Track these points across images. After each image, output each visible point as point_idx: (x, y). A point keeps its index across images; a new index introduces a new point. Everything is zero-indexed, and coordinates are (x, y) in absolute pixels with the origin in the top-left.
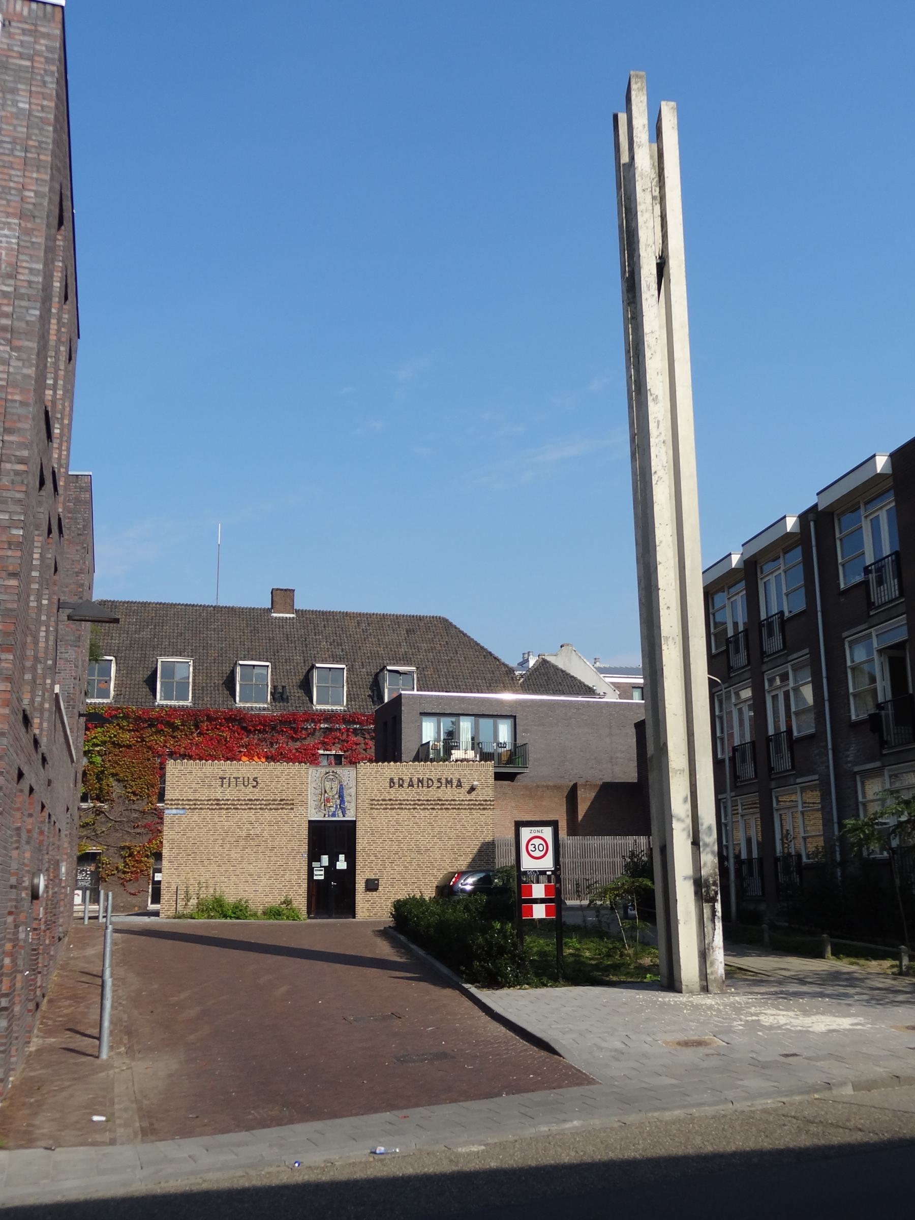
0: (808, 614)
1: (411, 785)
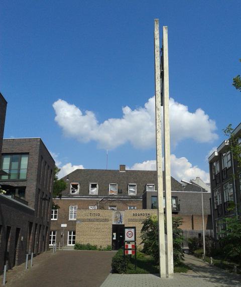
0: (231, 168)
1: (139, 215)
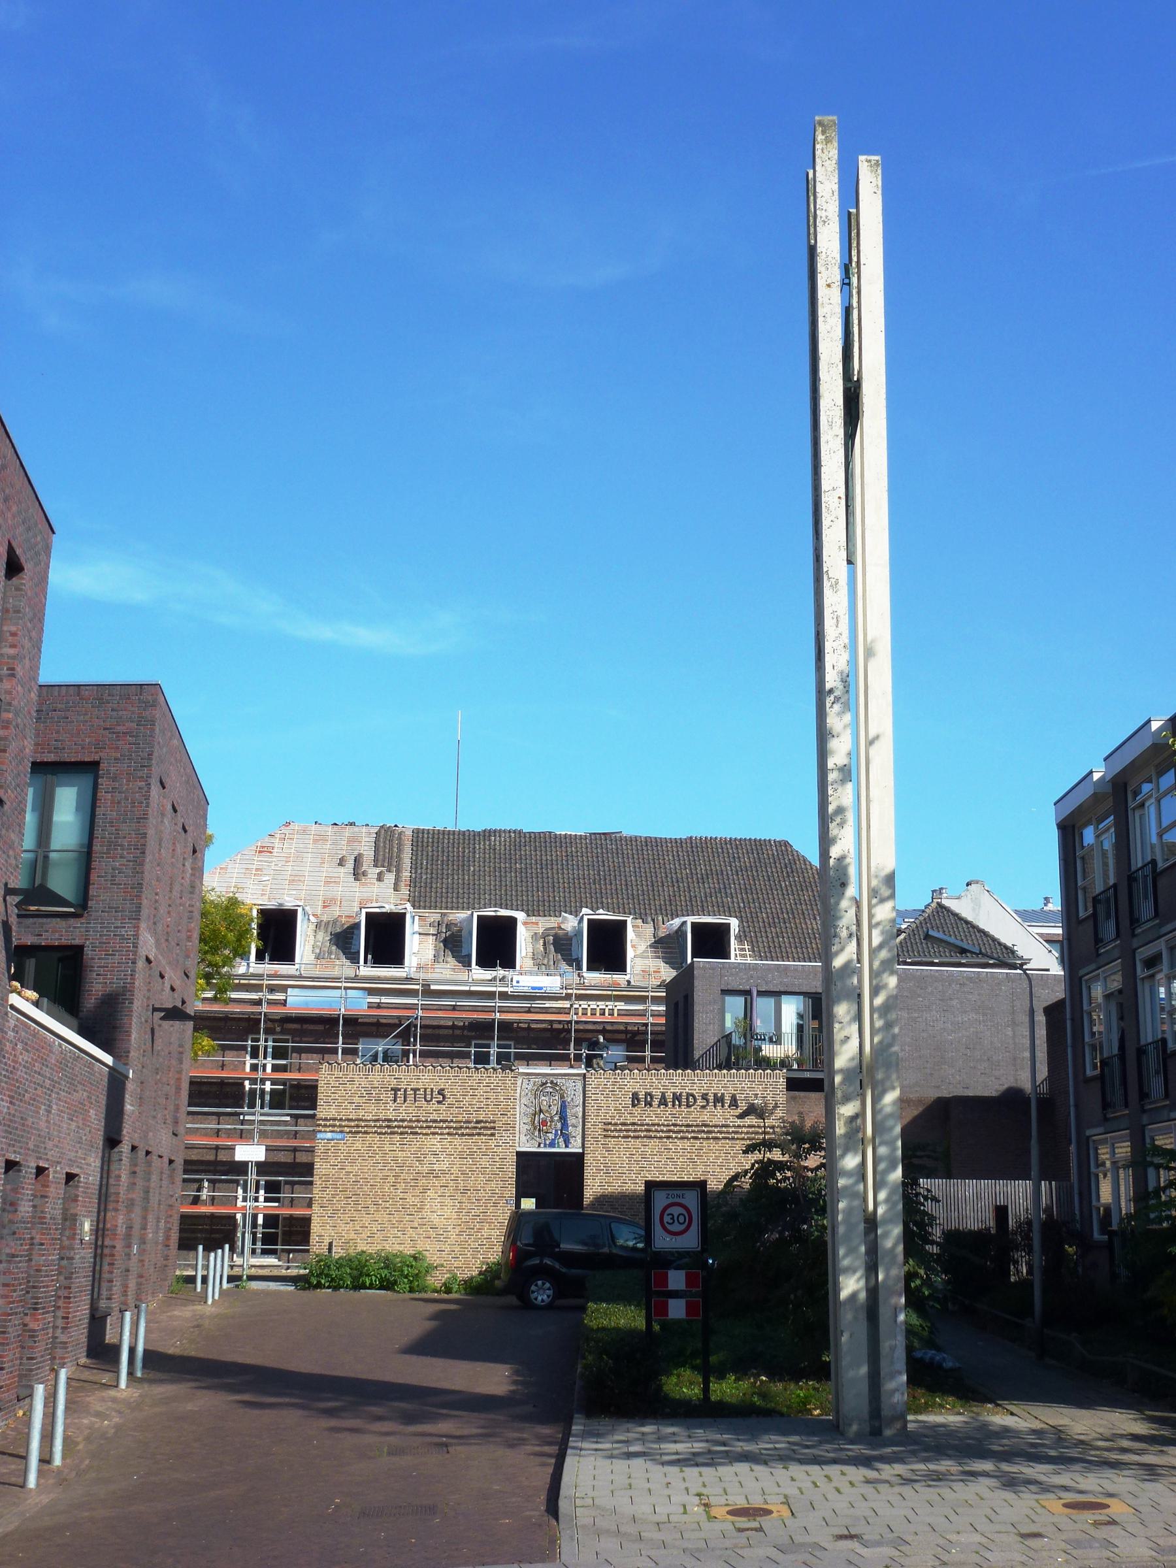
1: (663, 1102)
